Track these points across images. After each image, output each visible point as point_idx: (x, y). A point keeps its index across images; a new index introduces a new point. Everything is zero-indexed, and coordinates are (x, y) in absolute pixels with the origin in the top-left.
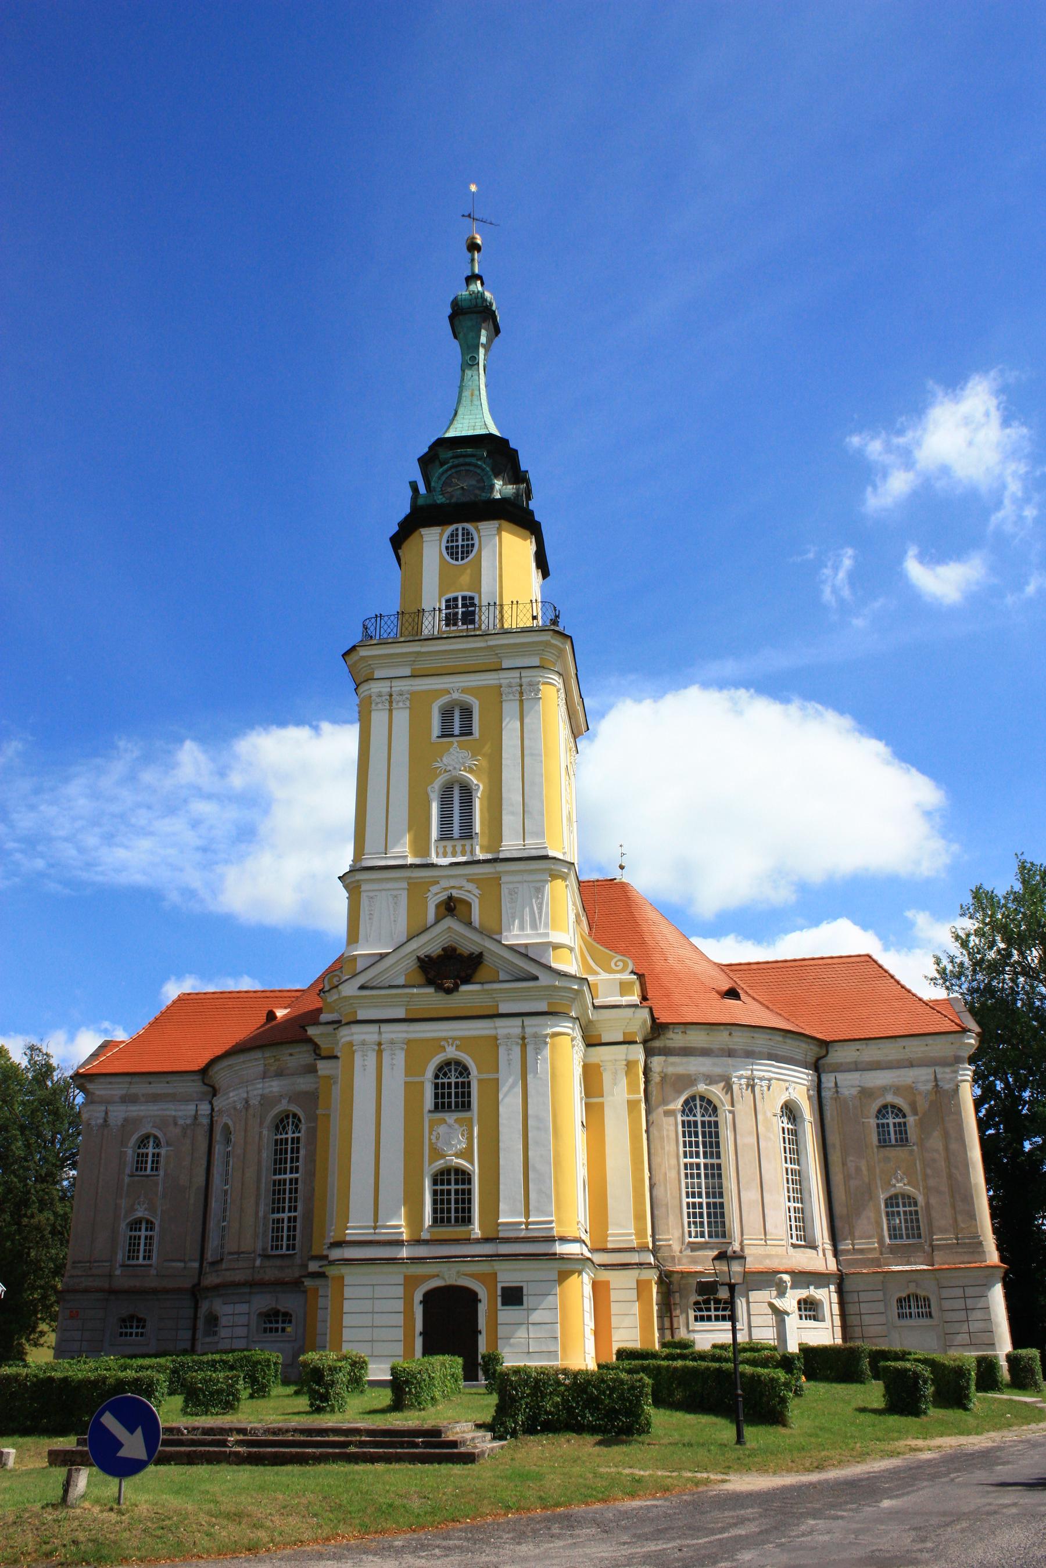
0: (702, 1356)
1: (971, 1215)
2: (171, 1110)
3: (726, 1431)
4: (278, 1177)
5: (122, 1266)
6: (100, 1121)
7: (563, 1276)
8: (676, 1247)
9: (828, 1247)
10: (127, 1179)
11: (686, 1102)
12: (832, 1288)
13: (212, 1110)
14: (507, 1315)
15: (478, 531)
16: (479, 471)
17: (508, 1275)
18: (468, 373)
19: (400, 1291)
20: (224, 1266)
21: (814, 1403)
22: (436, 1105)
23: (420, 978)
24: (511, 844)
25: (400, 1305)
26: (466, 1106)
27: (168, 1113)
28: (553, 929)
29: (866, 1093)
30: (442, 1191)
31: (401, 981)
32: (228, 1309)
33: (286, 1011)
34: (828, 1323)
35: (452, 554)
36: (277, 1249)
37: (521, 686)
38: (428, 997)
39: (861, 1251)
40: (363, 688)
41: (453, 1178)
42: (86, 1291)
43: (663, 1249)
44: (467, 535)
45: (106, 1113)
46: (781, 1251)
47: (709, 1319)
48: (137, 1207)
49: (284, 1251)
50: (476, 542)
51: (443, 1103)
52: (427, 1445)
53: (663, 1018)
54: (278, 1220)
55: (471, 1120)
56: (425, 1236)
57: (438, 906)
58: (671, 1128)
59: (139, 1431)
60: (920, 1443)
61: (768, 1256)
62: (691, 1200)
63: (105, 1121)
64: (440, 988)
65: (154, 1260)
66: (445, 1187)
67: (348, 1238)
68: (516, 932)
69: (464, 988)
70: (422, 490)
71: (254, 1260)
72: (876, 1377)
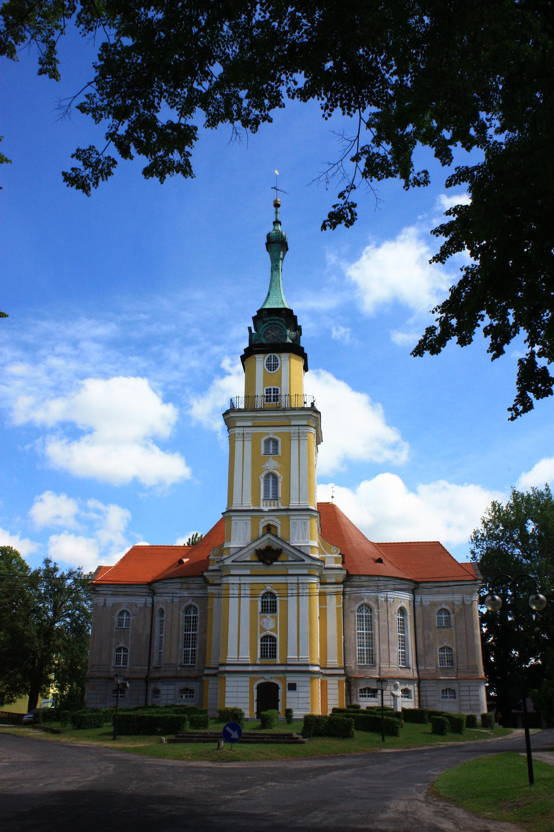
0: (364, 712)
1: (474, 656)
2: (133, 600)
3: (379, 738)
4: (186, 633)
5: (114, 667)
6: (103, 604)
7: (312, 679)
8: (353, 667)
9: (415, 668)
10: (115, 630)
11: (359, 607)
12: (416, 685)
13: (153, 601)
14: (290, 694)
15: (280, 357)
16: (280, 327)
17: (291, 679)
18: (275, 273)
19: (248, 684)
20: (162, 669)
21: (407, 730)
22: (262, 610)
23: (256, 558)
24: (294, 504)
25: (248, 689)
26: (275, 611)
27: (133, 601)
28: (311, 539)
29: (434, 604)
30: (264, 645)
31: (248, 559)
32: (166, 687)
33: (187, 560)
34: (413, 700)
35: (269, 368)
36: (186, 663)
37: (299, 433)
38: (260, 567)
39: (428, 670)
40: (231, 430)
41: (269, 639)
42: (99, 678)
43: (348, 668)
44: (276, 359)
45: (105, 601)
46: (395, 670)
47: (365, 696)
48: (120, 642)
49: (190, 664)
50: (279, 362)
51: (265, 609)
52: (288, 739)
53: (352, 572)
54: (187, 651)
55: (277, 616)
56: (258, 662)
57: (263, 528)
58: (353, 618)
59: (236, 731)
60: (441, 743)
61: (390, 672)
62: (360, 648)
63: (105, 604)
64: (265, 563)
65: (128, 665)
66: (266, 643)
67: (227, 662)
68: (295, 540)
69: (274, 563)
70: (253, 331)
71: (177, 667)
72: (430, 722)
